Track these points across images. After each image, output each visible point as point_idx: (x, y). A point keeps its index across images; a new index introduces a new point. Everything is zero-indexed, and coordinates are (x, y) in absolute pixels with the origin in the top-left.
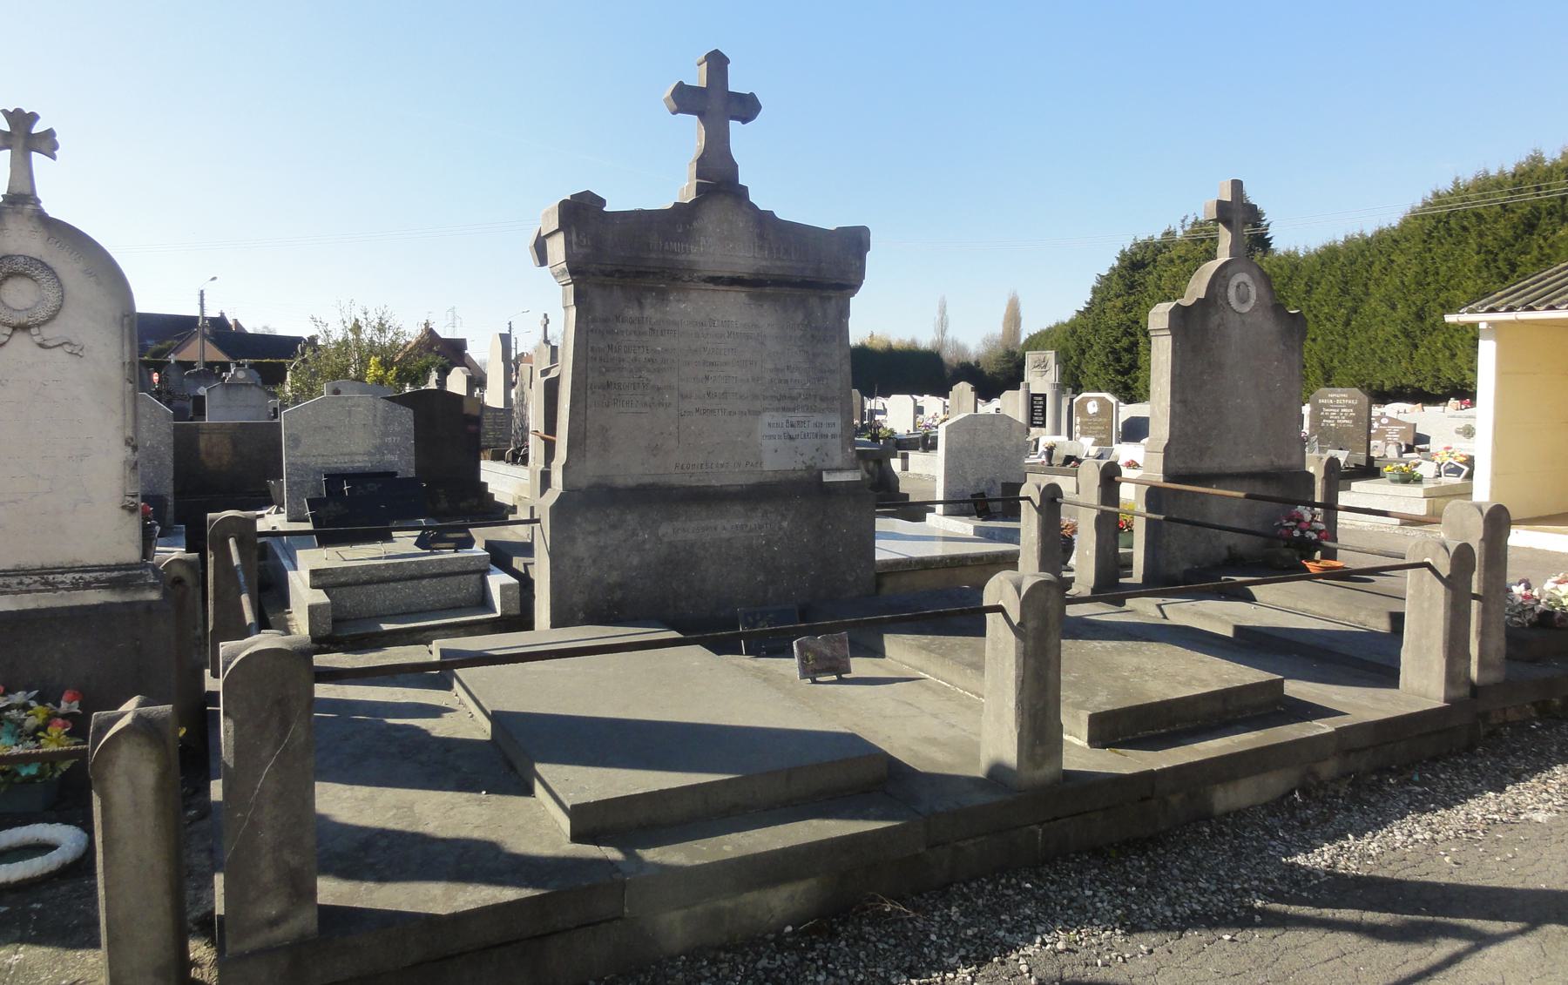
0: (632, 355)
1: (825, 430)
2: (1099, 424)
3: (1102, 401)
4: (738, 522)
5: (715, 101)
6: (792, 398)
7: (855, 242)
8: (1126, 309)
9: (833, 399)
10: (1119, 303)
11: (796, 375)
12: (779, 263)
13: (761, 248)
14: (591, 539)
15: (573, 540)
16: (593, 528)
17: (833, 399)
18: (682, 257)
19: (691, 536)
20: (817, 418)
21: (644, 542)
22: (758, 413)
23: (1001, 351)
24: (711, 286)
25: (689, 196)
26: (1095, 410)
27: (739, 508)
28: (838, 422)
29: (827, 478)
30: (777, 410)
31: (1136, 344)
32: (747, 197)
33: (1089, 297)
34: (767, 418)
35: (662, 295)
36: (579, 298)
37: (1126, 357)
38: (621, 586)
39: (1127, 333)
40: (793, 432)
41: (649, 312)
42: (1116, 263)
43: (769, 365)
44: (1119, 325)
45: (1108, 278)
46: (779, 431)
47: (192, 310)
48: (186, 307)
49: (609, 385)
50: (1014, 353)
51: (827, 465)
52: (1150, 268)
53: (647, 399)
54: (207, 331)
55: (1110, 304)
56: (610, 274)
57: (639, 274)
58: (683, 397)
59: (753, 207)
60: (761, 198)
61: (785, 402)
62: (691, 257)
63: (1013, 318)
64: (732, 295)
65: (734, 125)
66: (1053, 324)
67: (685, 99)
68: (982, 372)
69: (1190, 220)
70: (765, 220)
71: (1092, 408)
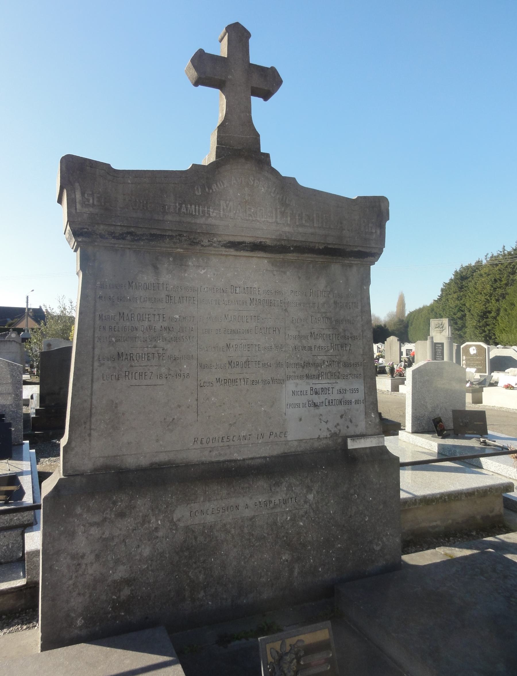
0: (146, 324)
1: (348, 396)
2: (477, 360)
3: (479, 348)
4: (262, 499)
5: (235, 73)
6: (316, 365)
7: (374, 212)
8: (459, 298)
9: (356, 365)
10: (455, 296)
11: (320, 342)
12: (301, 230)
13: (283, 214)
14: (94, 531)
15: (72, 535)
16: (96, 519)
17: (356, 365)
18: (201, 221)
19: (210, 519)
20: (341, 384)
21: (157, 529)
22: (281, 382)
23: (396, 320)
24: (232, 252)
25: (207, 156)
26: (475, 352)
27: (262, 483)
28: (361, 388)
29: (352, 445)
30: (301, 377)
31: (465, 315)
32: (269, 163)
33: (439, 293)
34: (291, 386)
35: (180, 261)
36: (86, 263)
37: (460, 322)
38: (128, 582)
39: (460, 310)
40: (317, 399)
41: (165, 278)
42: (453, 277)
43: (293, 332)
44: (456, 306)
45: (449, 284)
46: (304, 399)
47: (23, 305)
48: (19, 303)
49: (119, 355)
50: (403, 321)
51: (352, 430)
52: (470, 279)
53: (163, 370)
54: (31, 314)
55: (451, 297)
56: (122, 237)
57: (154, 237)
58: (202, 366)
59: (274, 172)
60: (281, 165)
61: (309, 369)
62: (210, 221)
63: (402, 304)
64: (255, 261)
65: (256, 102)
66: (421, 307)
67: (208, 71)
68: (387, 330)
69: (490, 255)
70: (287, 186)
71: (473, 351)
